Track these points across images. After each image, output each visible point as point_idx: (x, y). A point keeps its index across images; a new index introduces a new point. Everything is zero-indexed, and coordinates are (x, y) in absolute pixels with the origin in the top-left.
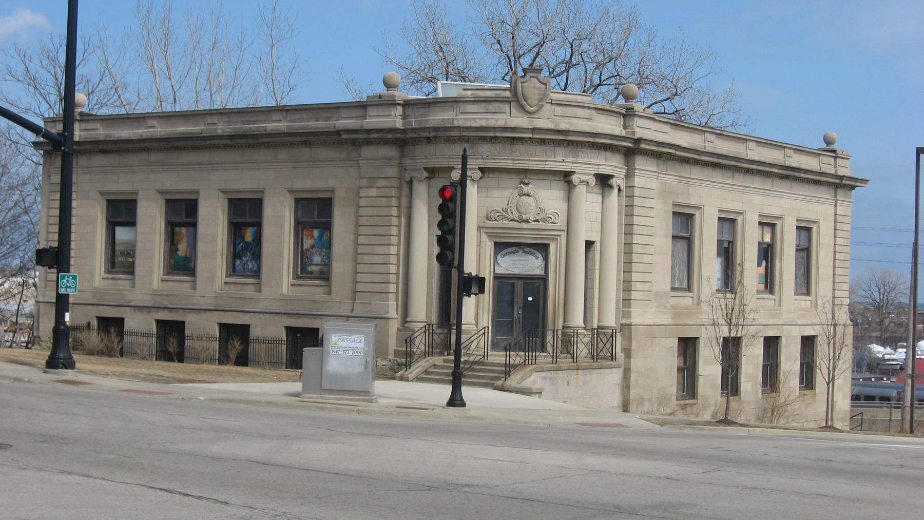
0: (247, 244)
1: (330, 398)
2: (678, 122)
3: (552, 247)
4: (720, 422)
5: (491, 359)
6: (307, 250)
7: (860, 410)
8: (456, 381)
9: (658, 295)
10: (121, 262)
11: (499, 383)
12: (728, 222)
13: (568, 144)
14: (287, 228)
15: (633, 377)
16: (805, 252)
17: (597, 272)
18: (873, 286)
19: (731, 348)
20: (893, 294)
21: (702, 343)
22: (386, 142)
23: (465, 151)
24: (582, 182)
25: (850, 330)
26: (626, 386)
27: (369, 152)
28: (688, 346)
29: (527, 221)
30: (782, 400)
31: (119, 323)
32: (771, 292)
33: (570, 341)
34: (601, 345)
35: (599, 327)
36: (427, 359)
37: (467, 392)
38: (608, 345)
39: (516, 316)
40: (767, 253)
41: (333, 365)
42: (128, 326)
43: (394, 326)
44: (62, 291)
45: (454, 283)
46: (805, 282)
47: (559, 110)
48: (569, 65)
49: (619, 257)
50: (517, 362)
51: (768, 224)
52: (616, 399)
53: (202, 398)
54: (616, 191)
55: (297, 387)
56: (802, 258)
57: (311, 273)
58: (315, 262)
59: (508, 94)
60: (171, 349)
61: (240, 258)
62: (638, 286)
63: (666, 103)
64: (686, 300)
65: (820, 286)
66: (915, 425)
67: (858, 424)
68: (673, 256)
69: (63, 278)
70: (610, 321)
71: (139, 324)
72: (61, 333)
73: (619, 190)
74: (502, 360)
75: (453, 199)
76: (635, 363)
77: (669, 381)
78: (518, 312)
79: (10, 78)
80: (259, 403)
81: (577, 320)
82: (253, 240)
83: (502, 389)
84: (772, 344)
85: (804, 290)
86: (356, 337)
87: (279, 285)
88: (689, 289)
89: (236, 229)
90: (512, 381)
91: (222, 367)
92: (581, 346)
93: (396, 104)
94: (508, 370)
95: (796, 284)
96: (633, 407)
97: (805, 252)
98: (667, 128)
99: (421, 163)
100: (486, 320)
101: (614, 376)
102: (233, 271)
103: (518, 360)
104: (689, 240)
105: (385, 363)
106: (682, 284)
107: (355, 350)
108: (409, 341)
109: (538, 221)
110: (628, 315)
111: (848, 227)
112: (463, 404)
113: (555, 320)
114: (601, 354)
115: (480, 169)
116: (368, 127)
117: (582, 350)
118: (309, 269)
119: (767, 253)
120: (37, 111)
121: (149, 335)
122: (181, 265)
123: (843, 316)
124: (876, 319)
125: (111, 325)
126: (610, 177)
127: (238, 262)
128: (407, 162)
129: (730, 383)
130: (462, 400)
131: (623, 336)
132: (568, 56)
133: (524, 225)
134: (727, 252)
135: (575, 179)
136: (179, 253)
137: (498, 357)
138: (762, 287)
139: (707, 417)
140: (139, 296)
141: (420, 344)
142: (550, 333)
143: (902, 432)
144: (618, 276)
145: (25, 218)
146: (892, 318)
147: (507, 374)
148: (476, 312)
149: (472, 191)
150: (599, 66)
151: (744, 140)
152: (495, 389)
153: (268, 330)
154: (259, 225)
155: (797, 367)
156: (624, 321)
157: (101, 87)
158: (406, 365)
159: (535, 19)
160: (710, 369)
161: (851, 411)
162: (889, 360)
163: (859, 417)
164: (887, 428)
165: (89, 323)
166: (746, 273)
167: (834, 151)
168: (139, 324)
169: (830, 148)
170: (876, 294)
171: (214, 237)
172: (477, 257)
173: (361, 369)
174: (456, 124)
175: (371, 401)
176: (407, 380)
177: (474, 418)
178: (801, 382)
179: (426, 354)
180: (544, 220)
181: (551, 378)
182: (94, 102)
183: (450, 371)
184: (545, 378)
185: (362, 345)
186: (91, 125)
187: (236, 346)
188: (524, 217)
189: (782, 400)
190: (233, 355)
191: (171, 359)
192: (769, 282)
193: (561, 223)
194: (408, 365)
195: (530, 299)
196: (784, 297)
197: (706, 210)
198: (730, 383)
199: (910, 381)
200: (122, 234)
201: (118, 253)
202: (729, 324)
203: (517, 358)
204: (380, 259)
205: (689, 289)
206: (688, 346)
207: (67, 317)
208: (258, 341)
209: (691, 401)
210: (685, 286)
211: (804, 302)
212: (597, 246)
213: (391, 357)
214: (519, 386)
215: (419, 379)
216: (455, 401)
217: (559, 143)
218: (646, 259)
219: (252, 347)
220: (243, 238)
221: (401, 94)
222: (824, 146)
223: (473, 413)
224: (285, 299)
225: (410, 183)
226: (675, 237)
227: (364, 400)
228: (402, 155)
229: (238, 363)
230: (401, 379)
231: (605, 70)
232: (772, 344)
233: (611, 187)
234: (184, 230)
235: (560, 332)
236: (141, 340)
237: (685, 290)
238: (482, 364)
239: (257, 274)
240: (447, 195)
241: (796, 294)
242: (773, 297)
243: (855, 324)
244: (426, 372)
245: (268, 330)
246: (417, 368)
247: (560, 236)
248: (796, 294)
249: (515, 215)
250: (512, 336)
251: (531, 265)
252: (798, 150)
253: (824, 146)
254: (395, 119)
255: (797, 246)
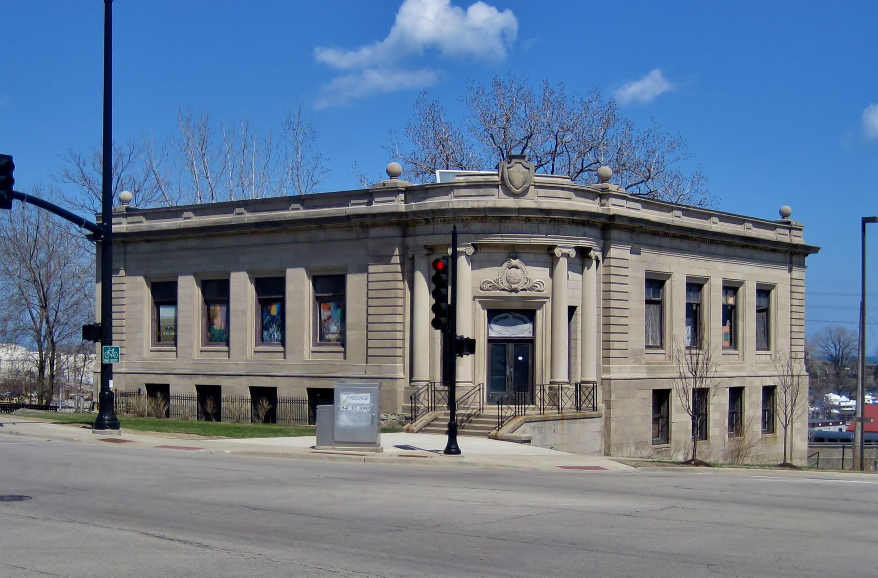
0: (273, 317)
1: (341, 449)
2: (649, 203)
3: (539, 313)
4: (687, 463)
5: (486, 412)
6: (325, 321)
7: (817, 450)
8: (452, 432)
9: (636, 354)
10: (165, 335)
11: (493, 432)
12: (695, 286)
13: (550, 221)
14: (307, 303)
15: (613, 425)
16: (764, 312)
17: (579, 334)
18: (830, 343)
19: (701, 395)
20: (847, 350)
21: (674, 394)
22: (391, 224)
23: (455, 228)
24: (564, 255)
25: (806, 381)
26: (607, 431)
27: (375, 232)
28: (661, 398)
29: (516, 291)
30: (746, 443)
31: (164, 389)
32: (736, 348)
33: (556, 395)
34: (583, 398)
35: (583, 382)
36: (430, 413)
37: (461, 441)
38: (590, 397)
39: (508, 373)
40: (730, 314)
41: (344, 421)
42: (172, 391)
43: (403, 385)
44: (106, 361)
45: (455, 347)
46: (765, 339)
47: (542, 192)
48: (554, 154)
49: (598, 319)
50: (508, 414)
51: (731, 288)
52: (598, 443)
53: (228, 452)
54: (594, 262)
55: (312, 440)
56: (762, 317)
57: (329, 340)
58: (332, 331)
59: (496, 178)
60: (209, 410)
61: (267, 330)
62: (617, 345)
63: (642, 185)
64: (659, 356)
65: (779, 341)
66: (865, 462)
67: (815, 463)
68: (647, 318)
69: (106, 350)
70: (592, 376)
71: (183, 389)
72: (107, 400)
73: (598, 261)
74: (495, 413)
75: (445, 270)
76: (614, 412)
77: (645, 426)
78: (510, 371)
79: (67, 180)
80: (278, 455)
81: (562, 376)
82: (278, 314)
83: (496, 438)
84: (736, 394)
85: (765, 345)
86: (363, 395)
87: (301, 352)
88: (662, 346)
89: (264, 303)
90: (504, 431)
91: (267, 426)
92: (565, 399)
93: (399, 192)
94: (501, 422)
95: (757, 341)
96: (613, 449)
97: (764, 312)
98: (639, 206)
99: (422, 241)
100: (482, 378)
101: (596, 425)
102: (261, 340)
103: (509, 413)
104: (660, 303)
105: (394, 417)
106: (655, 343)
107: (362, 406)
108: (414, 398)
109: (525, 290)
110: (608, 370)
111: (802, 290)
112: (458, 452)
113: (542, 376)
114: (584, 405)
115: (473, 245)
116: (374, 211)
117: (568, 403)
118: (327, 337)
119: (730, 314)
120: (91, 208)
121: (190, 399)
122: (217, 336)
123: (799, 368)
124: (835, 369)
125: (159, 391)
126: (589, 249)
127: (265, 333)
128: (409, 241)
129: (700, 429)
130: (457, 448)
131: (604, 389)
132: (554, 147)
133: (514, 294)
134: (694, 314)
135: (557, 252)
136: (215, 327)
137: (492, 410)
138: (727, 343)
139: (681, 458)
140: (182, 364)
141: (424, 402)
142: (538, 388)
143: (853, 469)
144: (598, 337)
145: (86, 302)
146: (847, 371)
147: (500, 425)
148: (472, 370)
149: (463, 264)
150: (582, 154)
151: (706, 216)
152: (490, 438)
153: (293, 391)
154: (282, 302)
155: (759, 413)
156: (604, 376)
157: (147, 185)
158: (412, 419)
159: (523, 115)
160: (681, 418)
161: (809, 452)
162: (844, 407)
163: (816, 457)
164: (842, 466)
165: (140, 390)
166: (713, 332)
167: (789, 223)
168: (183, 389)
169: (786, 220)
170: (833, 350)
171: (244, 312)
172: (470, 321)
173: (368, 423)
174: (451, 206)
175: (377, 451)
176: (413, 432)
177: (467, 464)
178: (764, 427)
179: (428, 409)
180: (531, 289)
181: (539, 428)
182: (140, 199)
183: (446, 423)
184: (534, 428)
185: (368, 402)
186: (136, 219)
187: (266, 406)
188: (513, 286)
189: (746, 443)
190: (262, 413)
191: (208, 418)
192: (733, 340)
193: (547, 292)
194: (412, 419)
195: (520, 358)
196: (747, 352)
197: (675, 276)
198: (700, 429)
199: (859, 424)
200: (166, 313)
201: (162, 329)
202: (695, 377)
203: (508, 410)
204: (388, 327)
205: (662, 346)
206: (661, 398)
207: (111, 384)
208: (286, 401)
209: (665, 445)
210: (658, 344)
211: (764, 357)
212: (579, 311)
213: (399, 411)
214: (510, 435)
215: (420, 431)
216: (452, 449)
217: (542, 221)
218: (623, 321)
219: (280, 407)
220: (269, 312)
221: (401, 183)
222: (780, 219)
223: (466, 459)
224: (306, 365)
225: (413, 259)
226: (648, 302)
227: (371, 451)
228: (405, 235)
229: (266, 421)
230: (408, 431)
231: (586, 158)
232: (736, 394)
233: (590, 258)
234: (218, 308)
235: (547, 387)
236: (184, 403)
237: (658, 347)
238: (478, 416)
239: (283, 342)
240: (440, 266)
241: (757, 349)
242: (736, 352)
243: (813, 375)
244: (428, 425)
245: (293, 391)
246: (420, 423)
247: (545, 302)
248: (757, 349)
249: (505, 285)
250: (504, 391)
251: (522, 330)
252: (758, 224)
253: (780, 219)
254: (398, 204)
255: (757, 307)
